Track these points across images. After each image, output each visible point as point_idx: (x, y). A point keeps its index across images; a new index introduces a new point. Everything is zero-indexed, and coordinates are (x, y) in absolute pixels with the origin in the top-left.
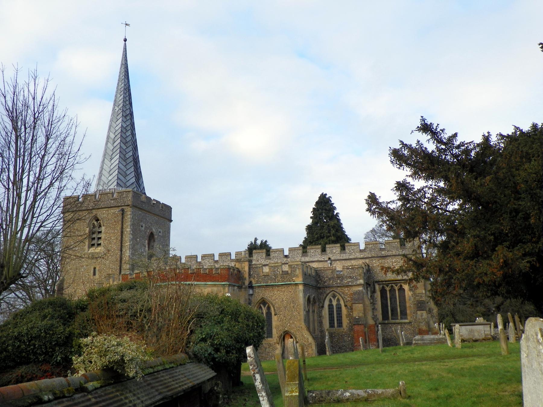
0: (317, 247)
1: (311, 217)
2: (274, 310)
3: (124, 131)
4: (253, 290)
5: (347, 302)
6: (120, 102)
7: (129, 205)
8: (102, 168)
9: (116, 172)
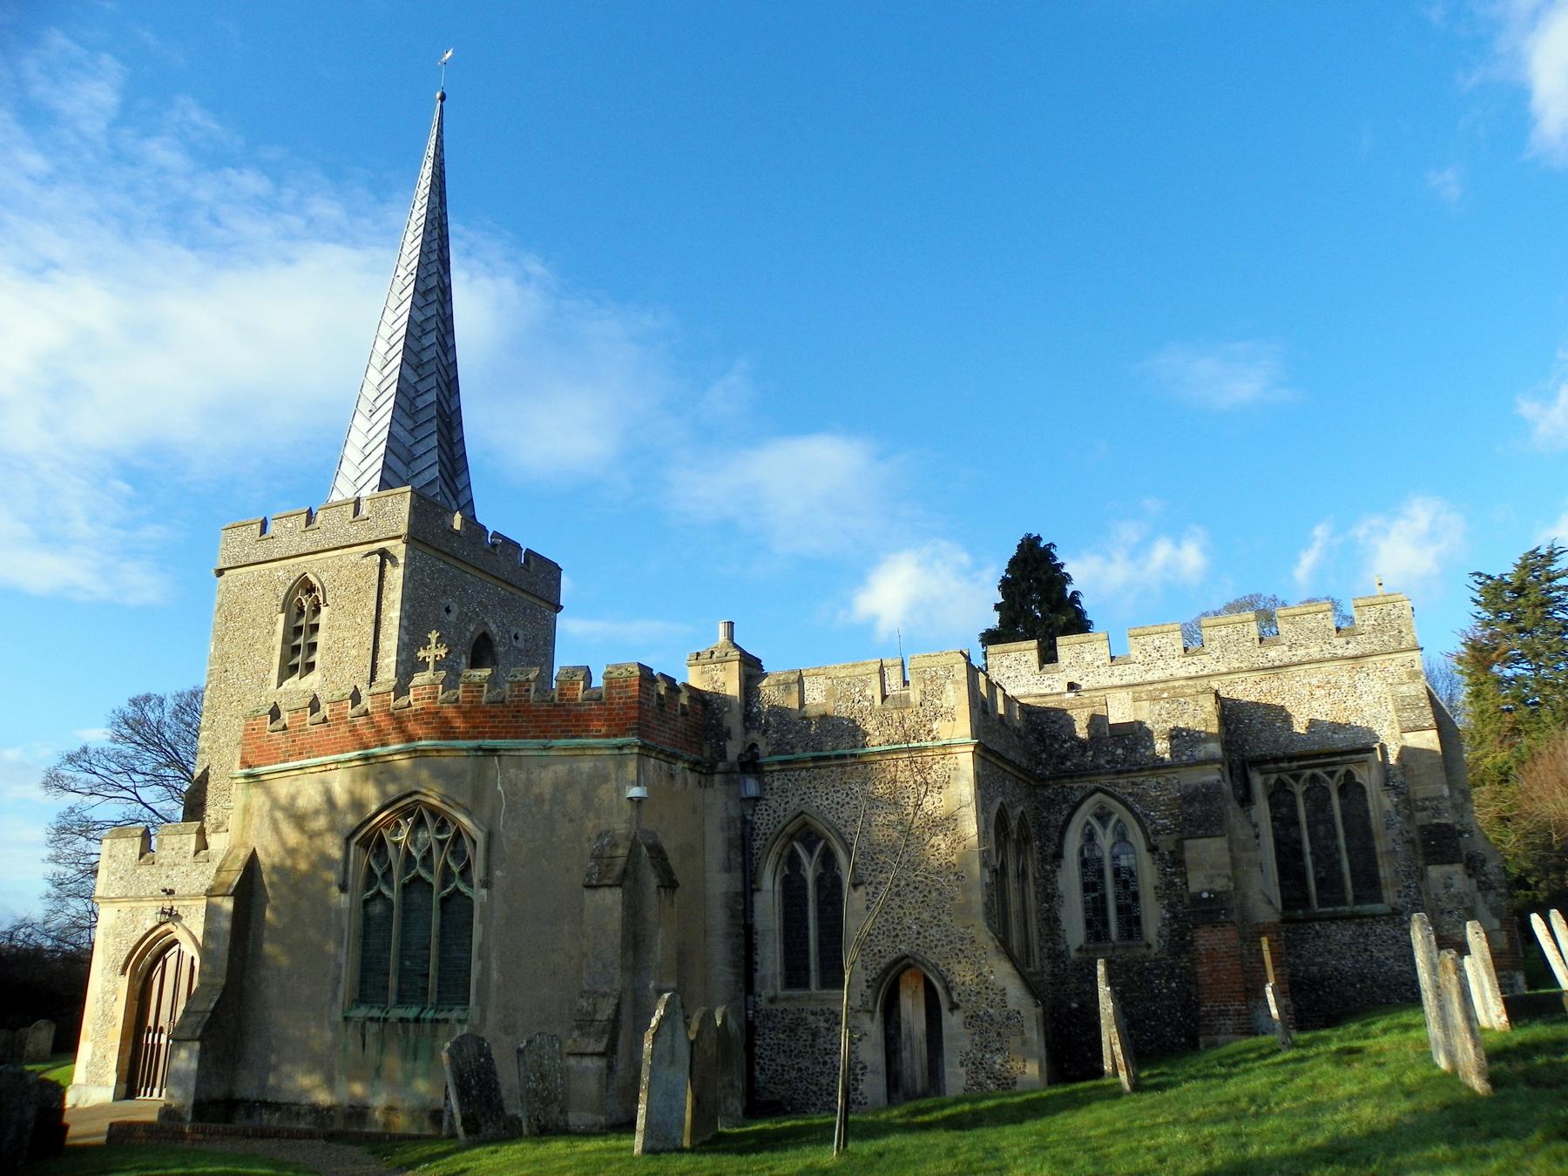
0: (1024, 644)
1: (997, 607)
3: (417, 332)
4: (759, 779)
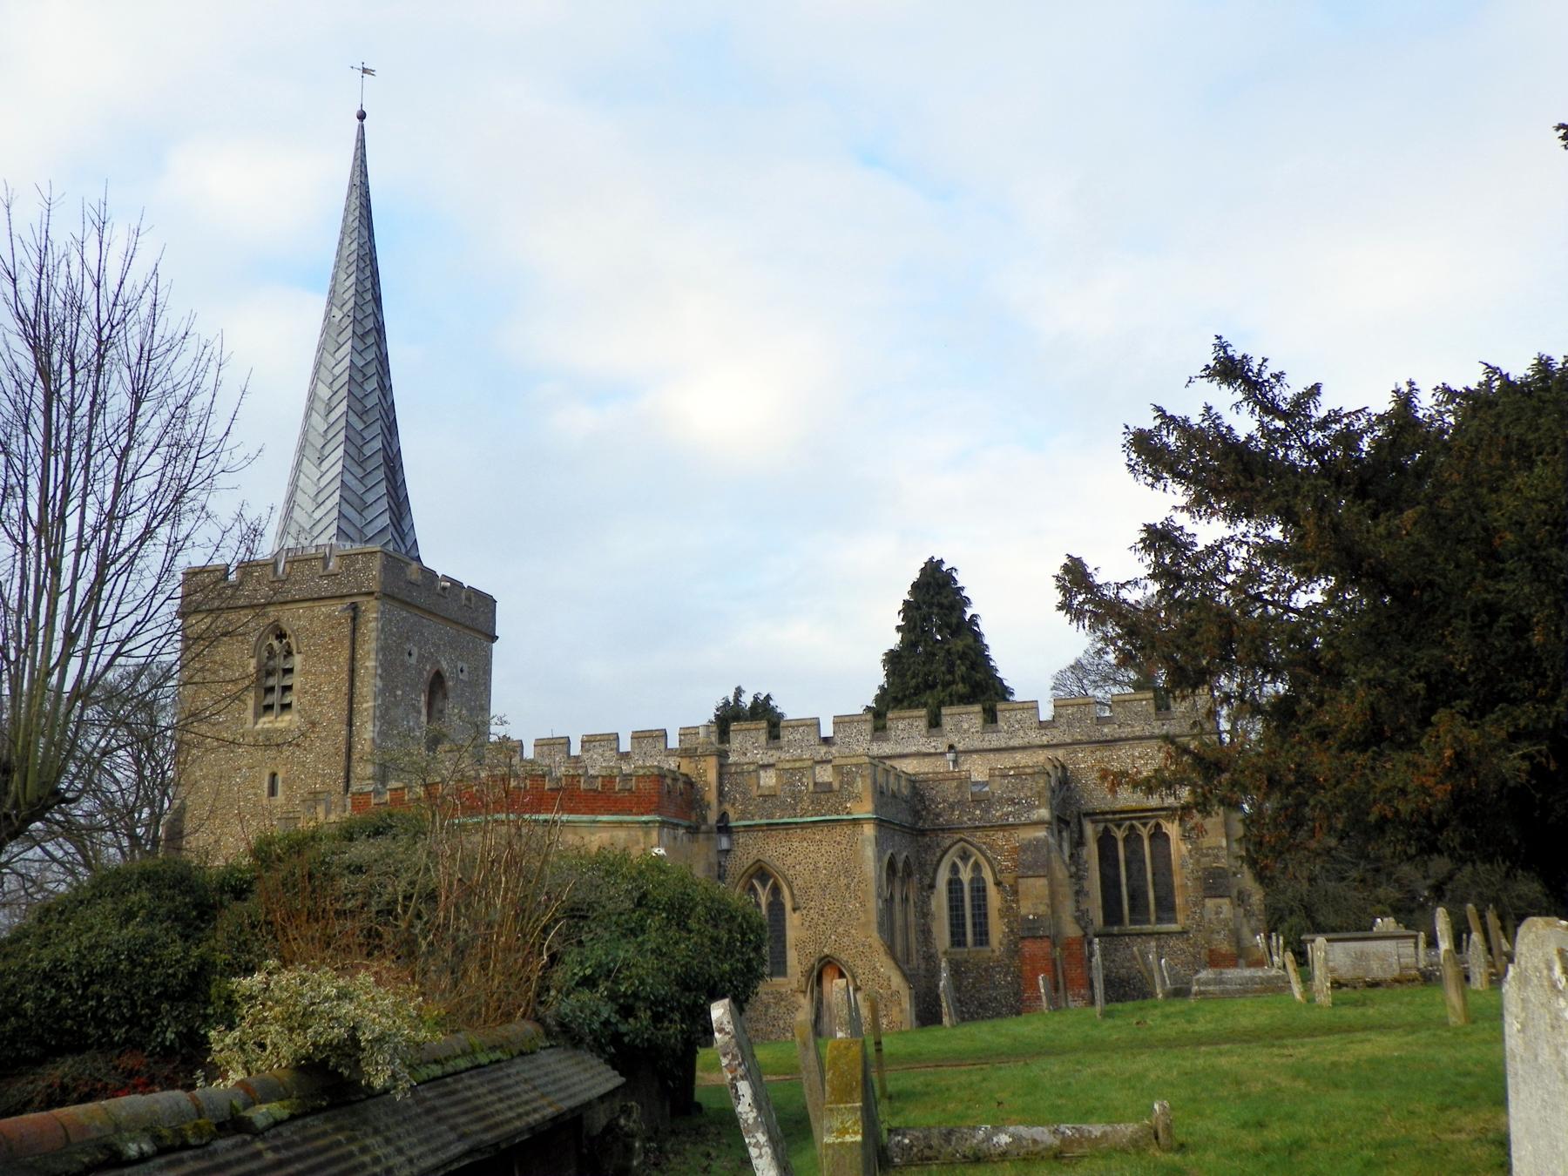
0: (916, 713)
1: (899, 628)
2: (792, 895)
3: (359, 378)
4: (730, 837)
5: (1001, 871)
6: (346, 296)
7: (371, 594)
8: (294, 486)
9: (336, 497)
